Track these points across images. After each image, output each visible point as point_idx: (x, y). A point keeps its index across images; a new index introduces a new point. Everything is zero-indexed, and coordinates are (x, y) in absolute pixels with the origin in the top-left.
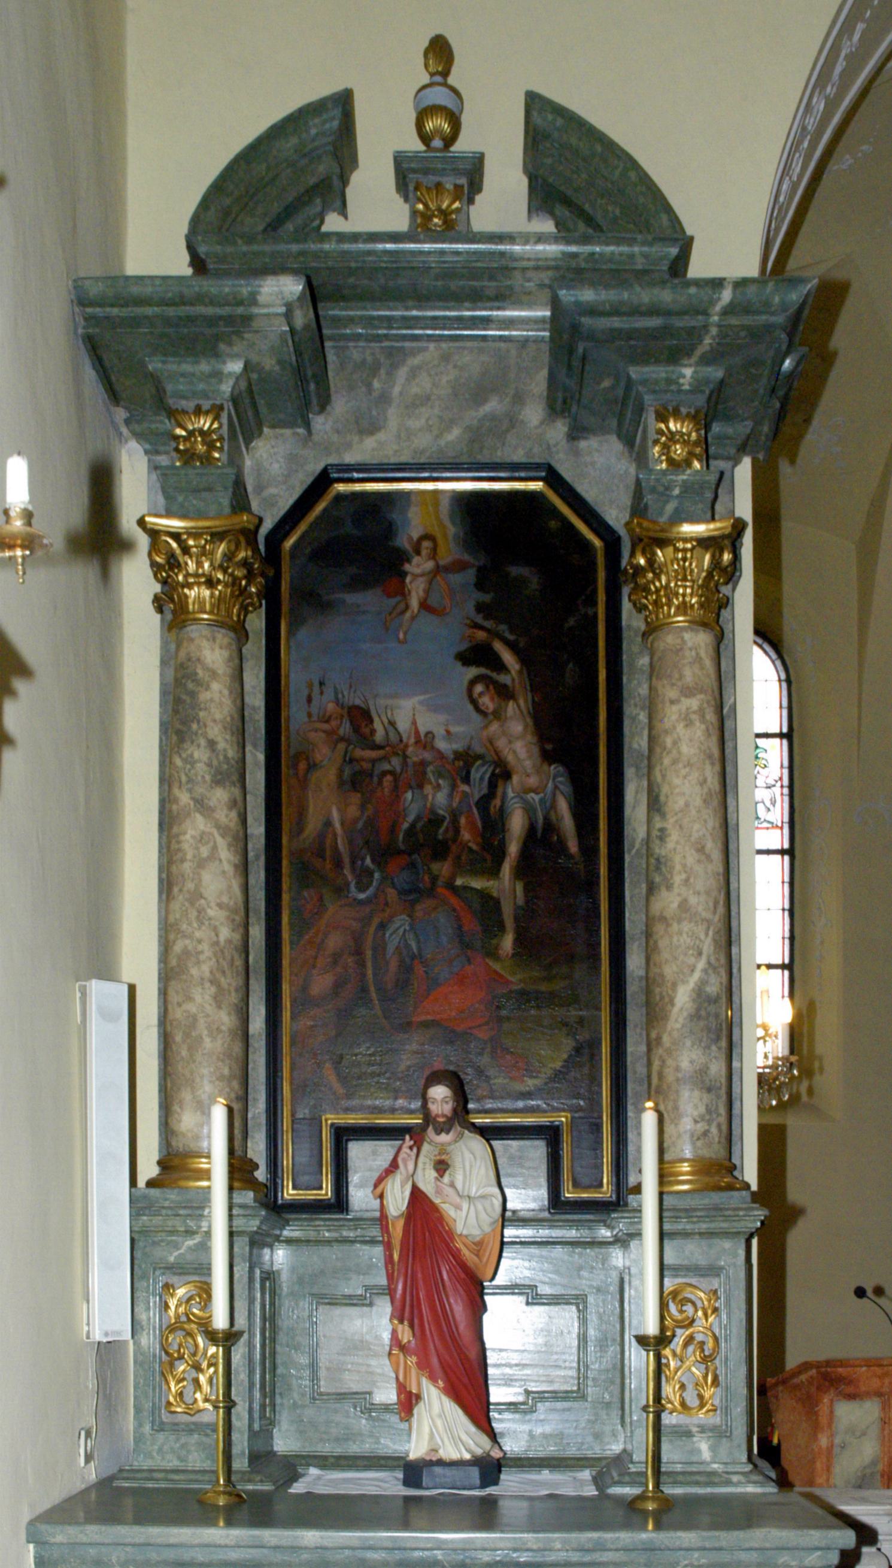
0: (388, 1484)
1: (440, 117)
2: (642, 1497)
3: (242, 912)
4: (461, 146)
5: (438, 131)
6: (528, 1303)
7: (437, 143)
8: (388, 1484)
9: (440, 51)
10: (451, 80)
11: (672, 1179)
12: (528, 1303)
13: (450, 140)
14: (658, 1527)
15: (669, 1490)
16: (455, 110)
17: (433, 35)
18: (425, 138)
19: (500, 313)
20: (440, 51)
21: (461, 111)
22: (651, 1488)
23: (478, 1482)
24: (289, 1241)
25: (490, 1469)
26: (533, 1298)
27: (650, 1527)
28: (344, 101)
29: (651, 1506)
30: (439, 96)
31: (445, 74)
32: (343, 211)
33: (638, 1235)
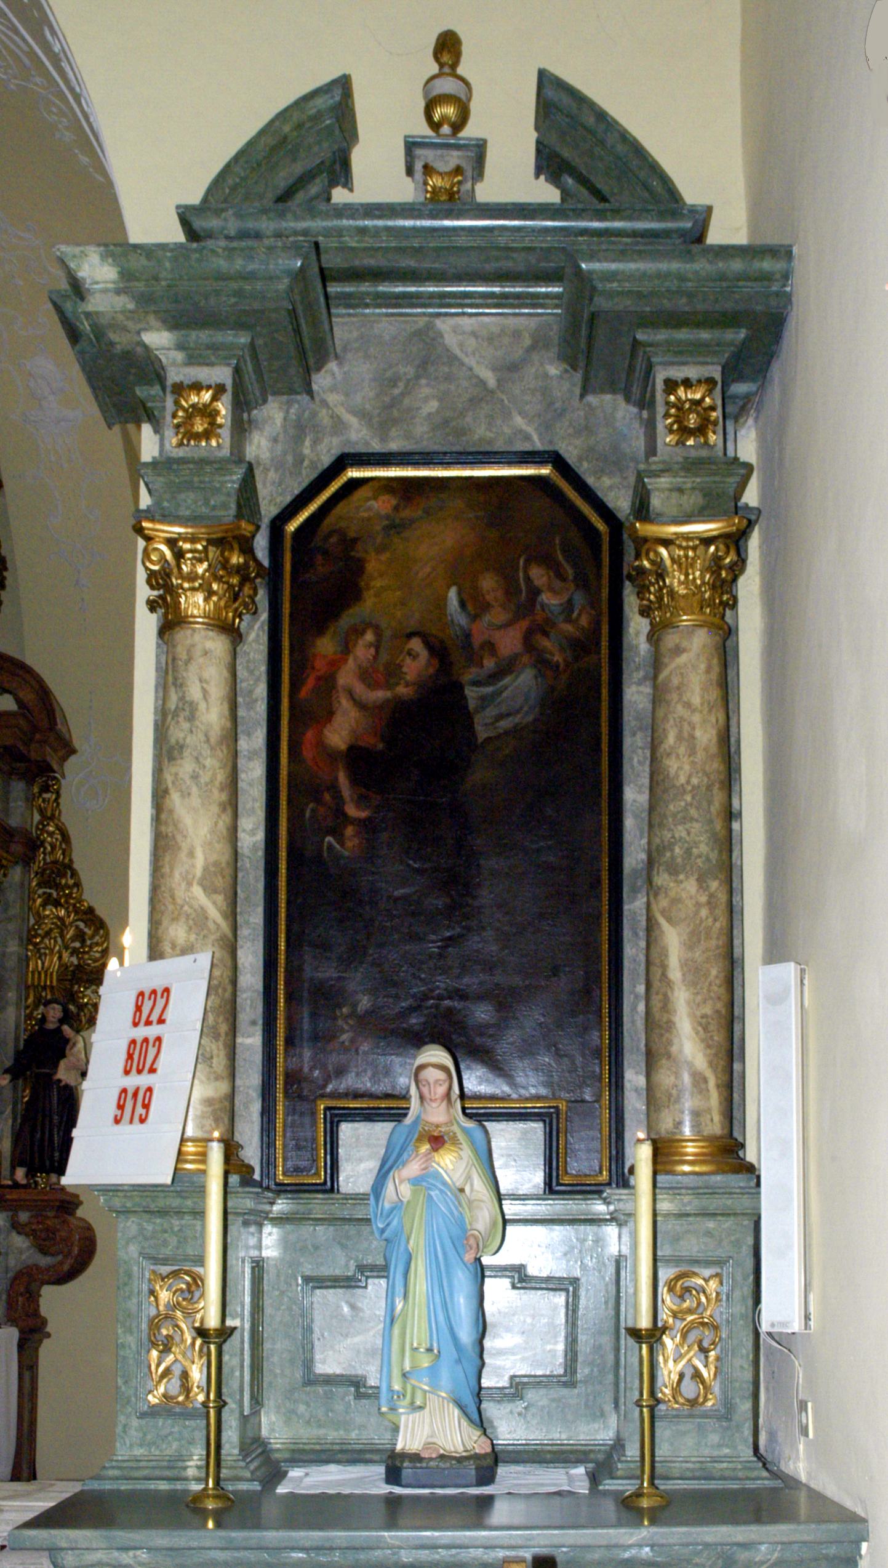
0: (369, 1480)
1: (447, 107)
2: (639, 1494)
3: (228, 872)
4: (470, 131)
5: (444, 119)
6: (514, 1287)
7: (446, 129)
8: (369, 1480)
9: (448, 47)
10: (460, 71)
11: (677, 1158)
12: (514, 1287)
13: (458, 126)
14: (218, 1525)
15: (663, 1485)
16: (463, 98)
17: (446, 29)
18: (435, 126)
19: (664, 266)
20: (448, 47)
21: (469, 100)
22: (211, 1485)
23: (474, 1482)
24: (280, 1221)
25: (487, 1465)
26: (520, 1282)
27: (211, 1524)
28: (344, 84)
29: (211, 1505)
30: (447, 85)
31: (454, 66)
32: (348, 184)
33: (631, 1215)
